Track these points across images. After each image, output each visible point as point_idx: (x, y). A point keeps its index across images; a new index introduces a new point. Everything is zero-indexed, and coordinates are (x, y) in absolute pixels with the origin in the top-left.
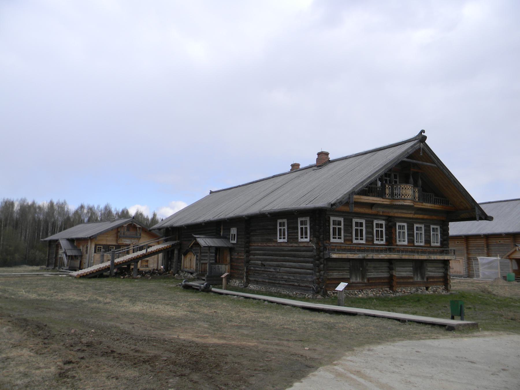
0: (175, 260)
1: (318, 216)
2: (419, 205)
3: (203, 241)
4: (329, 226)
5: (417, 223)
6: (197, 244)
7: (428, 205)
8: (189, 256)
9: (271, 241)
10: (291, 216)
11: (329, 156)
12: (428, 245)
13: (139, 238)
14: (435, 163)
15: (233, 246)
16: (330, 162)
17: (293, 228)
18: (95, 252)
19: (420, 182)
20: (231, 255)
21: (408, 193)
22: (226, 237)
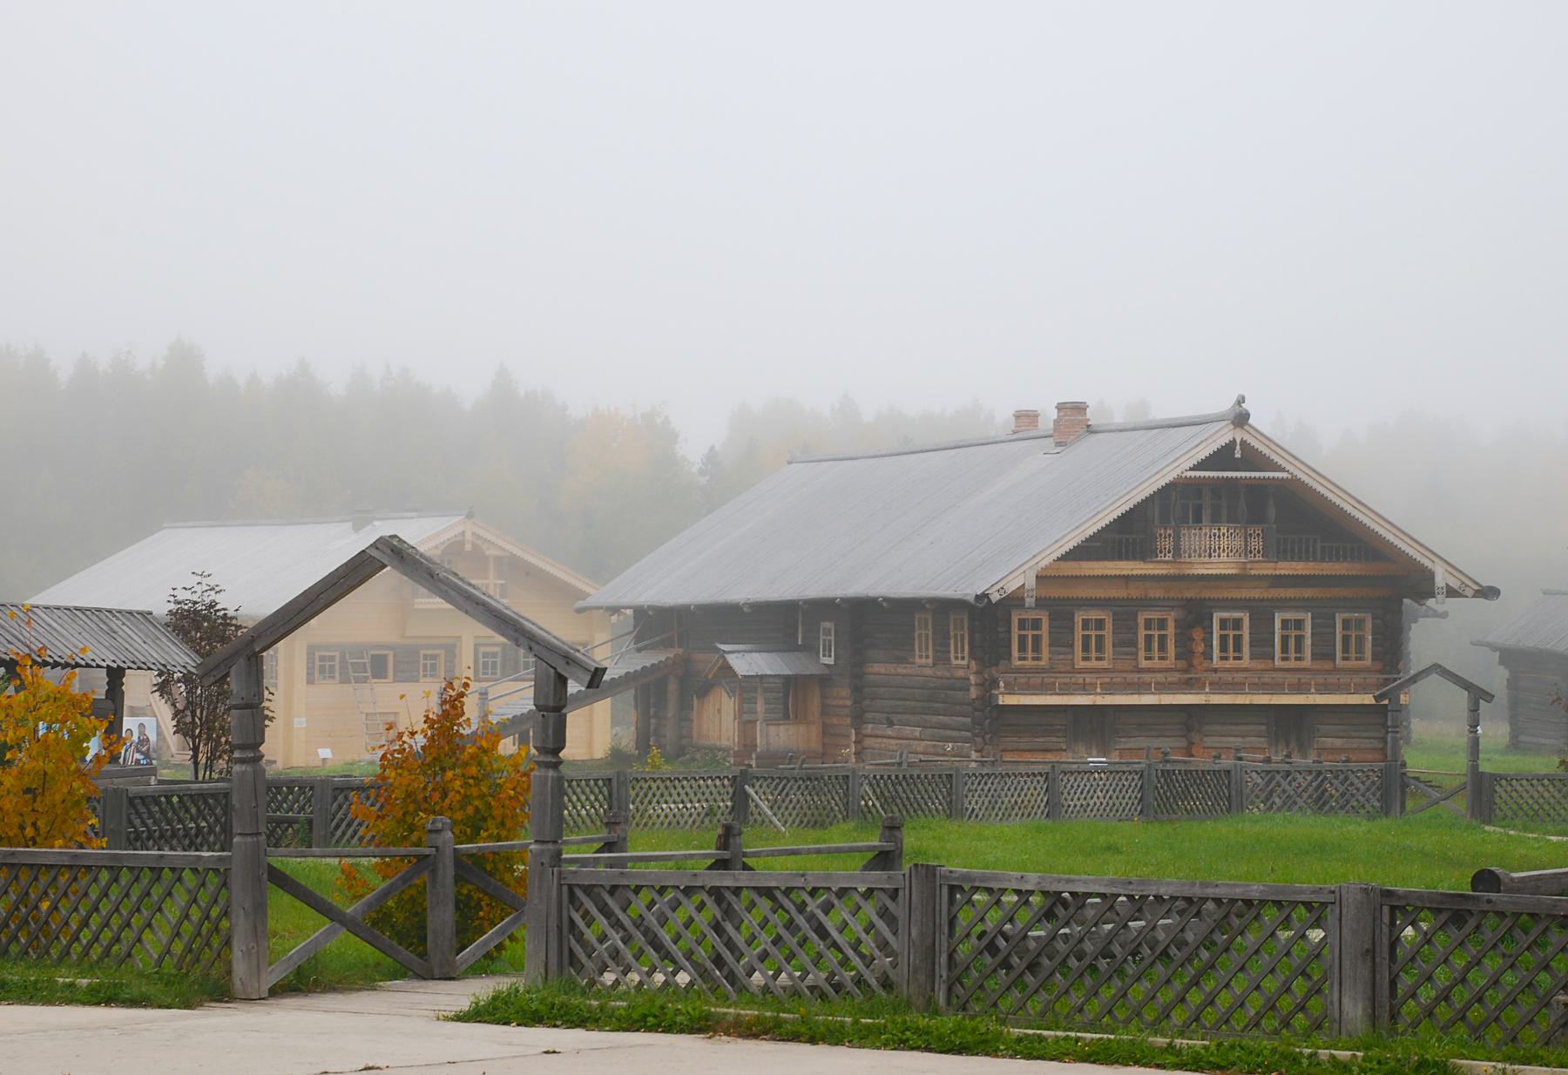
0: (671, 710)
1: (986, 622)
2: (1268, 569)
3: (747, 662)
4: (1009, 631)
5: (1281, 608)
6: (727, 668)
7: (1285, 568)
8: (712, 698)
9: (901, 660)
10: (944, 608)
11: (1089, 414)
12: (1328, 665)
13: (1274, 1051)
14: (1283, 470)
15: (826, 671)
16: (1091, 431)
17: (942, 639)
18: (310, 681)
19: (1272, 512)
20: (823, 696)
21: (1216, 554)
22: (810, 648)
